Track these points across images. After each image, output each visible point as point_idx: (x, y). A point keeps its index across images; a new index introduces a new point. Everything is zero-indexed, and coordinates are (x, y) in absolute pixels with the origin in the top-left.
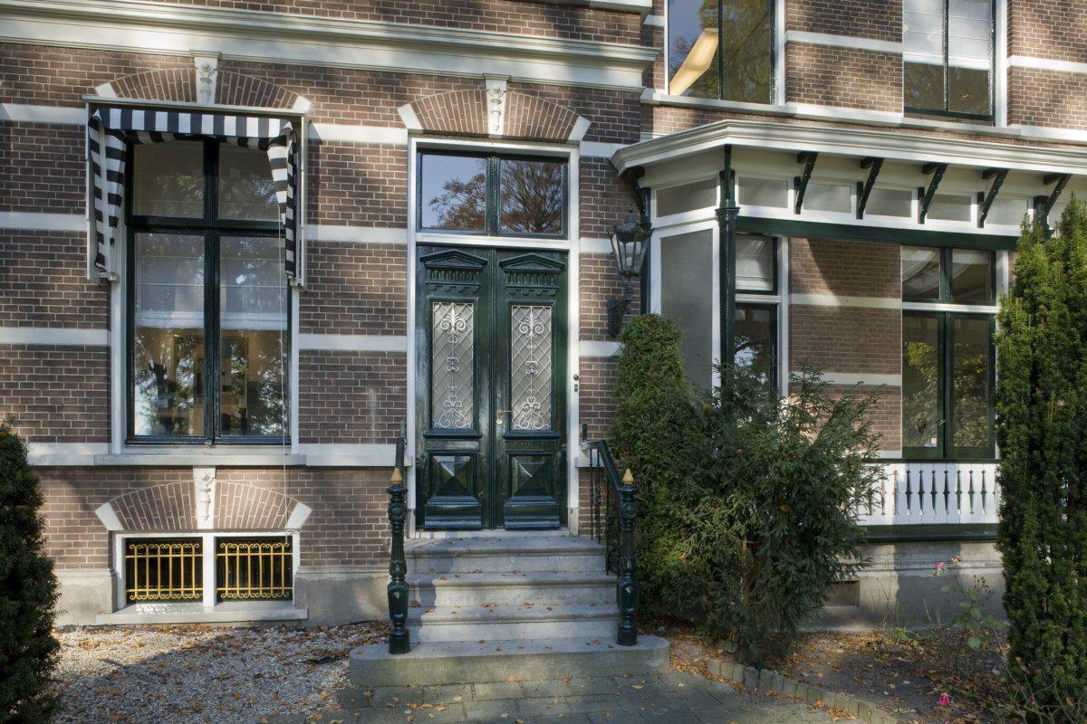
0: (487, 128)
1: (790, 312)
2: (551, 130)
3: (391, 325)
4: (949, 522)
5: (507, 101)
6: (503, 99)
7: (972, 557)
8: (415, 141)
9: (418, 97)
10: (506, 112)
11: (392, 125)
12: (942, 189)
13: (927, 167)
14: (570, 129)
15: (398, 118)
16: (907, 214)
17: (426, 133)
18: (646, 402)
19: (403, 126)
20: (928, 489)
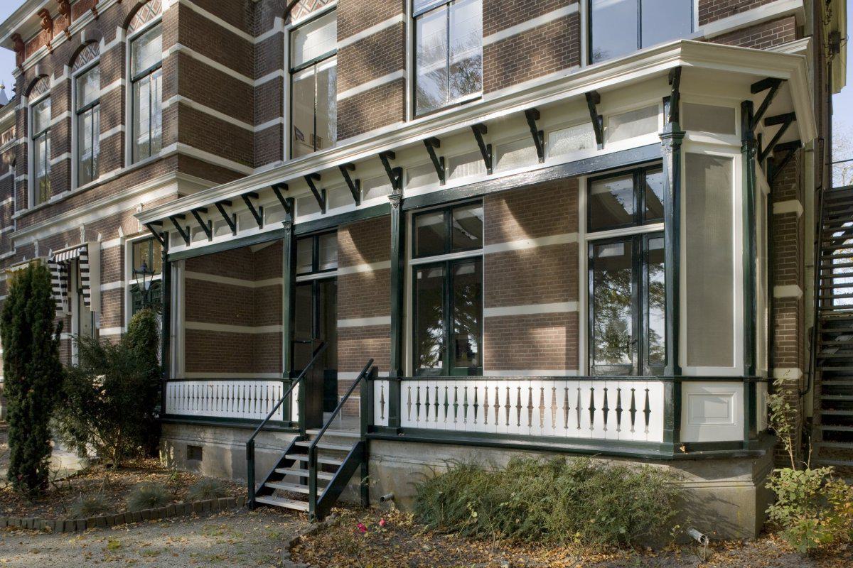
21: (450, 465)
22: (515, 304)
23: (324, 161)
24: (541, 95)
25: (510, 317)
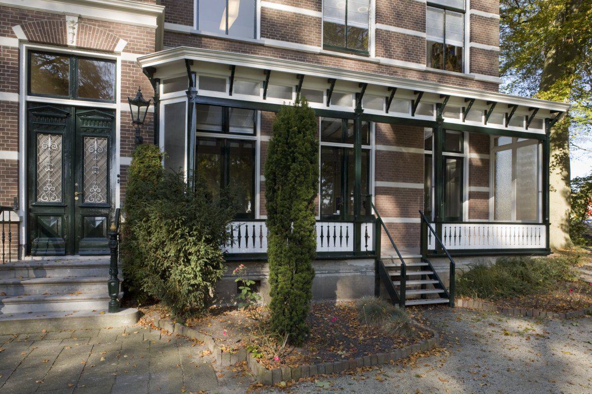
0: (66, 42)
1: (376, 154)
2: (104, 45)
3: (8, 145)
4: (329, 251)
5: (79, 28)
6: (76, 26)
7: (321, 268)
8: (25, 45)
9: (24, 22)
10: (78, 34)
11: (8, 36)
12: (448, 105)
13: (531, 109)
14: (115, 45)
15: (12, 32)
16: (481, 121)
17: (30, 42)
18: (137, 189)
19: (15, 37)
20: (453, 235)
21: (470, 266)
22: (393, 181)
23: (440, 89)
24: (498, 98)
25: (391, 188)
